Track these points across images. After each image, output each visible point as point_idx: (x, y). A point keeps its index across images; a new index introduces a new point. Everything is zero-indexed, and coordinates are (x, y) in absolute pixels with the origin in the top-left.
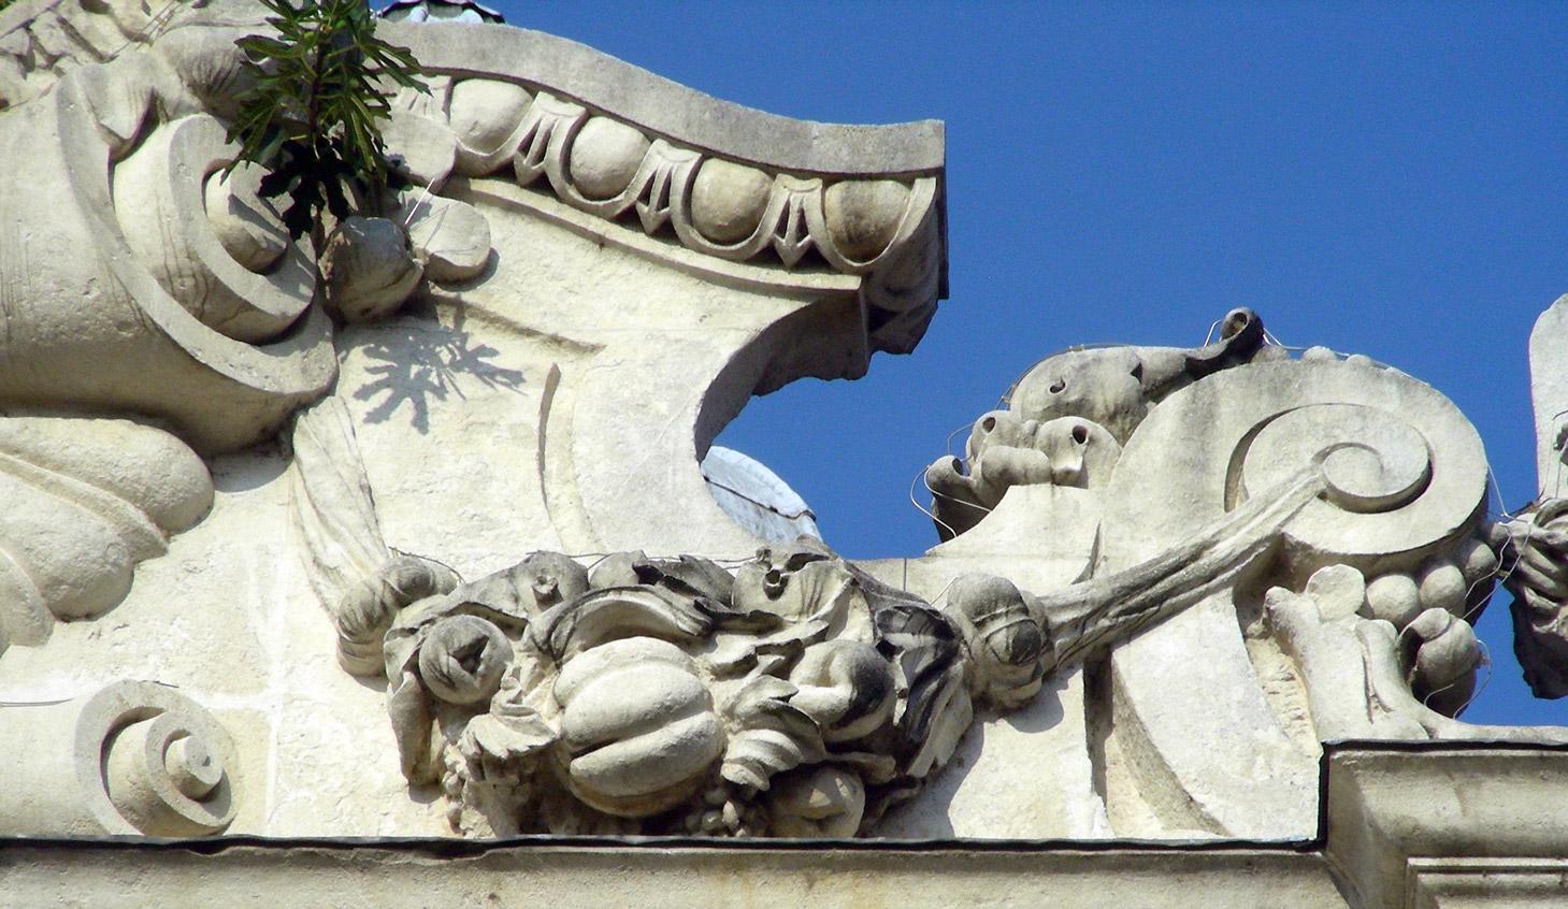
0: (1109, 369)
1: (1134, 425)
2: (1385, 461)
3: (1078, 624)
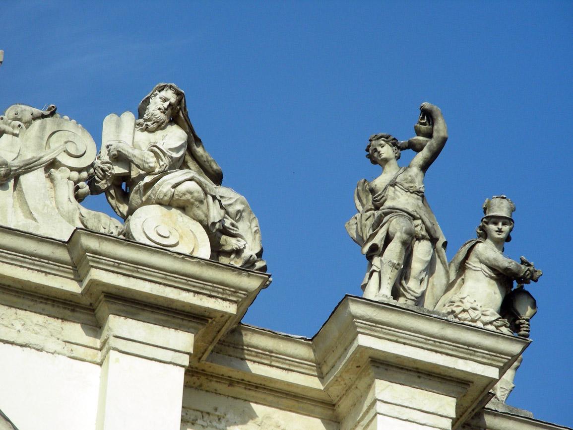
0: (28, 111)
1: (30, 126)
2: (78, 147)
3: (16, 170)
